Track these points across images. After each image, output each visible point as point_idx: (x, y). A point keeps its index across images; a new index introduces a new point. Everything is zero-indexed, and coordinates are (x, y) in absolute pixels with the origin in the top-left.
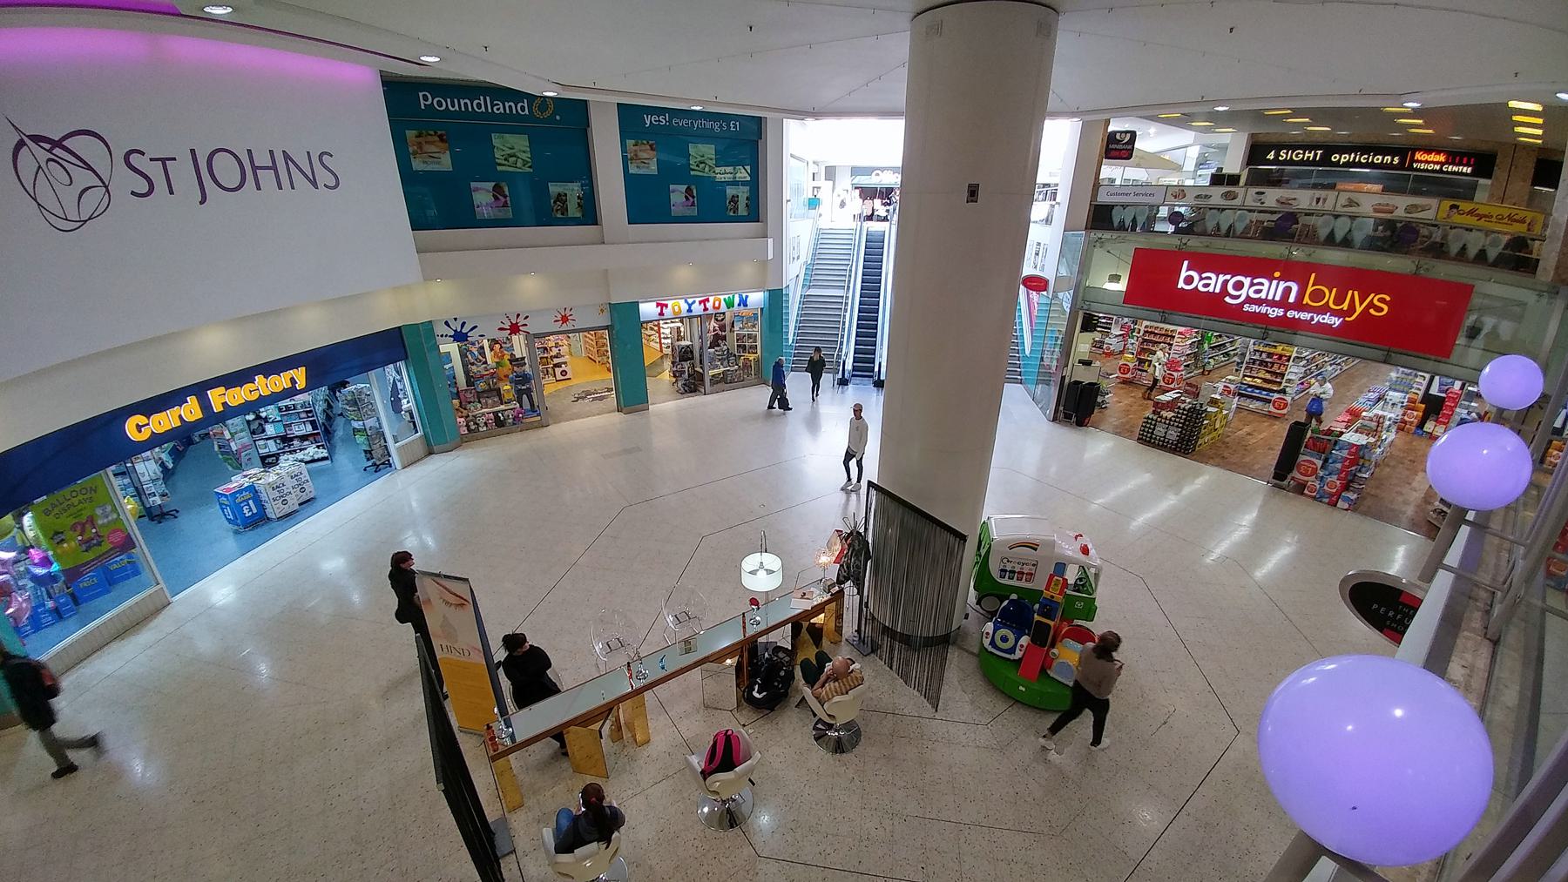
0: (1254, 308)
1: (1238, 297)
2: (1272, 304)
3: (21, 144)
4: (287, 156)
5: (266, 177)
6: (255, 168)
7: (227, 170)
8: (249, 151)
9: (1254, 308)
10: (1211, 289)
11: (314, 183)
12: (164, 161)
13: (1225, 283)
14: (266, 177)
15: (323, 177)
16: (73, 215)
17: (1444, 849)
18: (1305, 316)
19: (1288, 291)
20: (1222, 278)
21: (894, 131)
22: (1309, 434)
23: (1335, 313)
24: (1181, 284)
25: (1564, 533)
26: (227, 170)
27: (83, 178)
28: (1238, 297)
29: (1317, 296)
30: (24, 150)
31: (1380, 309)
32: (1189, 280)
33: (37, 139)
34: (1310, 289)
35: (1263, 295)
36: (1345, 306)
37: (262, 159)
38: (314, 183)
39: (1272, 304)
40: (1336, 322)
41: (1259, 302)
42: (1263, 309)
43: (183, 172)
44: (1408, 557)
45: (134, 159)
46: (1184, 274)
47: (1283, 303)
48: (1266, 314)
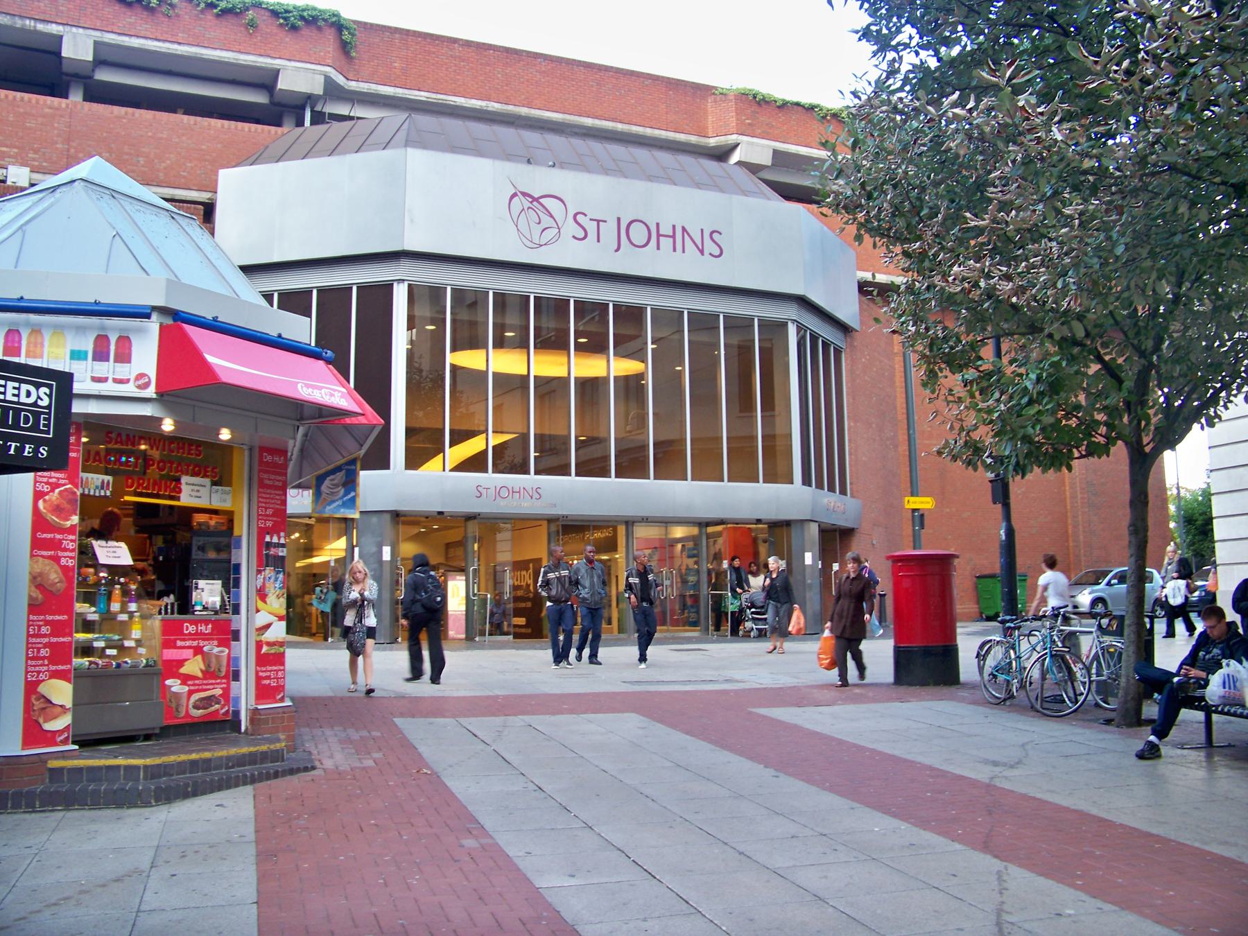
3: (514, 195)
4: (684, 229)
5: (666, 243)
6: (659, 235)
7: (638, 234)
8: (658, 224)
11: (702, 252)
12: (598, 221)
14: (666, 243)
15: (710, 247)
17: (987, 710)
21: (74, 410)
25: (130, 5)
26: (638, 234)
27: (547, 221)
30: (516, 199)
37: (666, 229)
38: (702, 252)
43: (609, 230)
45: (579, 218)
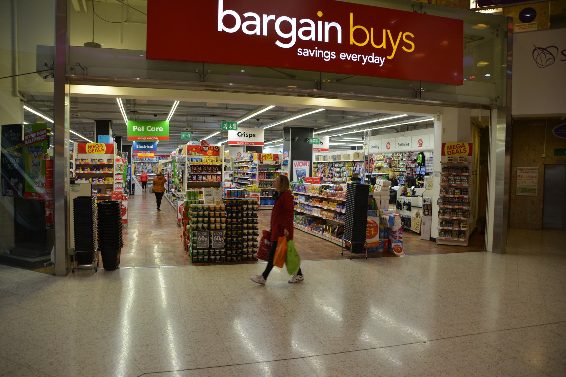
0: (307, 52)
1: (288, 41)
2: (322, 46)
9: (307, 52)
10: (257, 31)
13: (271, 24)
16: (544, 64)
18: (355, 57)
19: (333, 31)
20: (267, 19)
22: (96, 201)
23: (379, 53)
24: (221, 27)
27: (549, 56)
28: (288, 41)
29: (360, 35)
30: (536, 51)
31: (409, 47)
32: (229, 21)
33: (539, 48)
34: (352, 30)
35: (312, 37)
36: (384, 45)
39: (322, 46)
40: (379, 60)
41: (310, 45)
42: (317, 53)
44: (165, 276)
46: (221, 14)
47: (332, 45)
48: (321, 59)
